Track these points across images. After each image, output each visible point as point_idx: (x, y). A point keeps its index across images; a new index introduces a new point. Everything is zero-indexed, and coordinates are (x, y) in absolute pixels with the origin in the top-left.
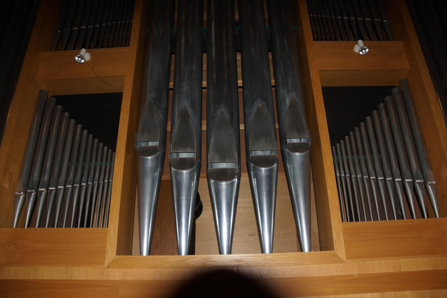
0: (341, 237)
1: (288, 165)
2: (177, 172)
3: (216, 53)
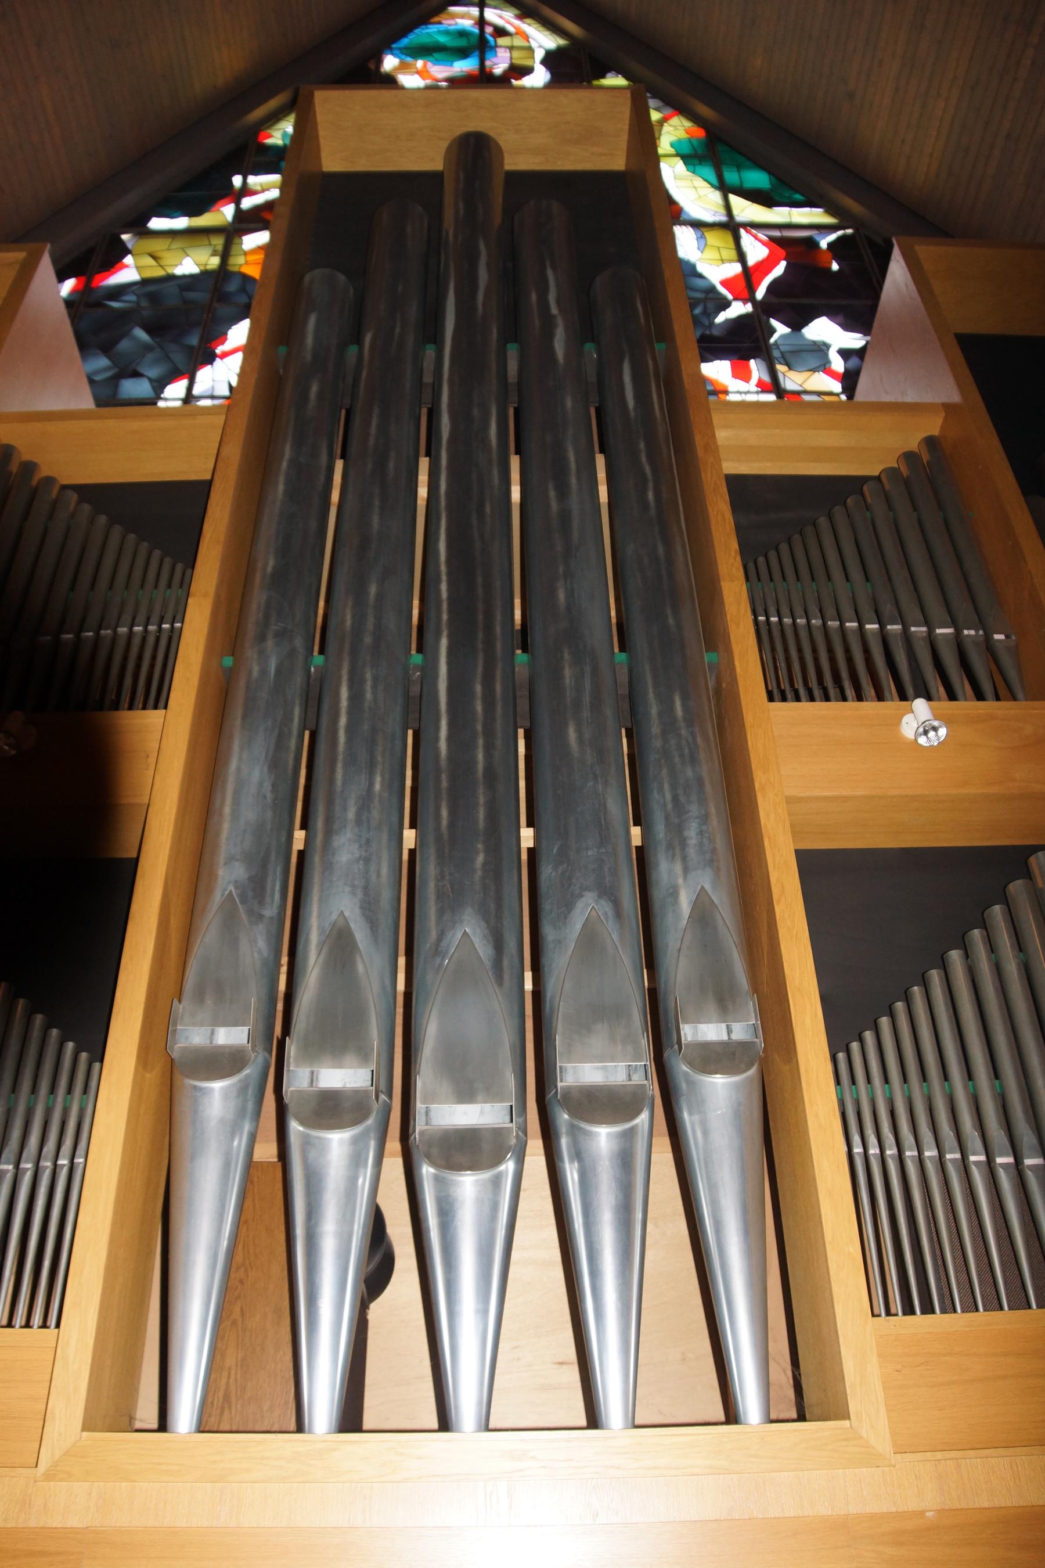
0: (874, 1369)
1: (686, 1115)
2: (308, 1136)
3: (450, 739)
